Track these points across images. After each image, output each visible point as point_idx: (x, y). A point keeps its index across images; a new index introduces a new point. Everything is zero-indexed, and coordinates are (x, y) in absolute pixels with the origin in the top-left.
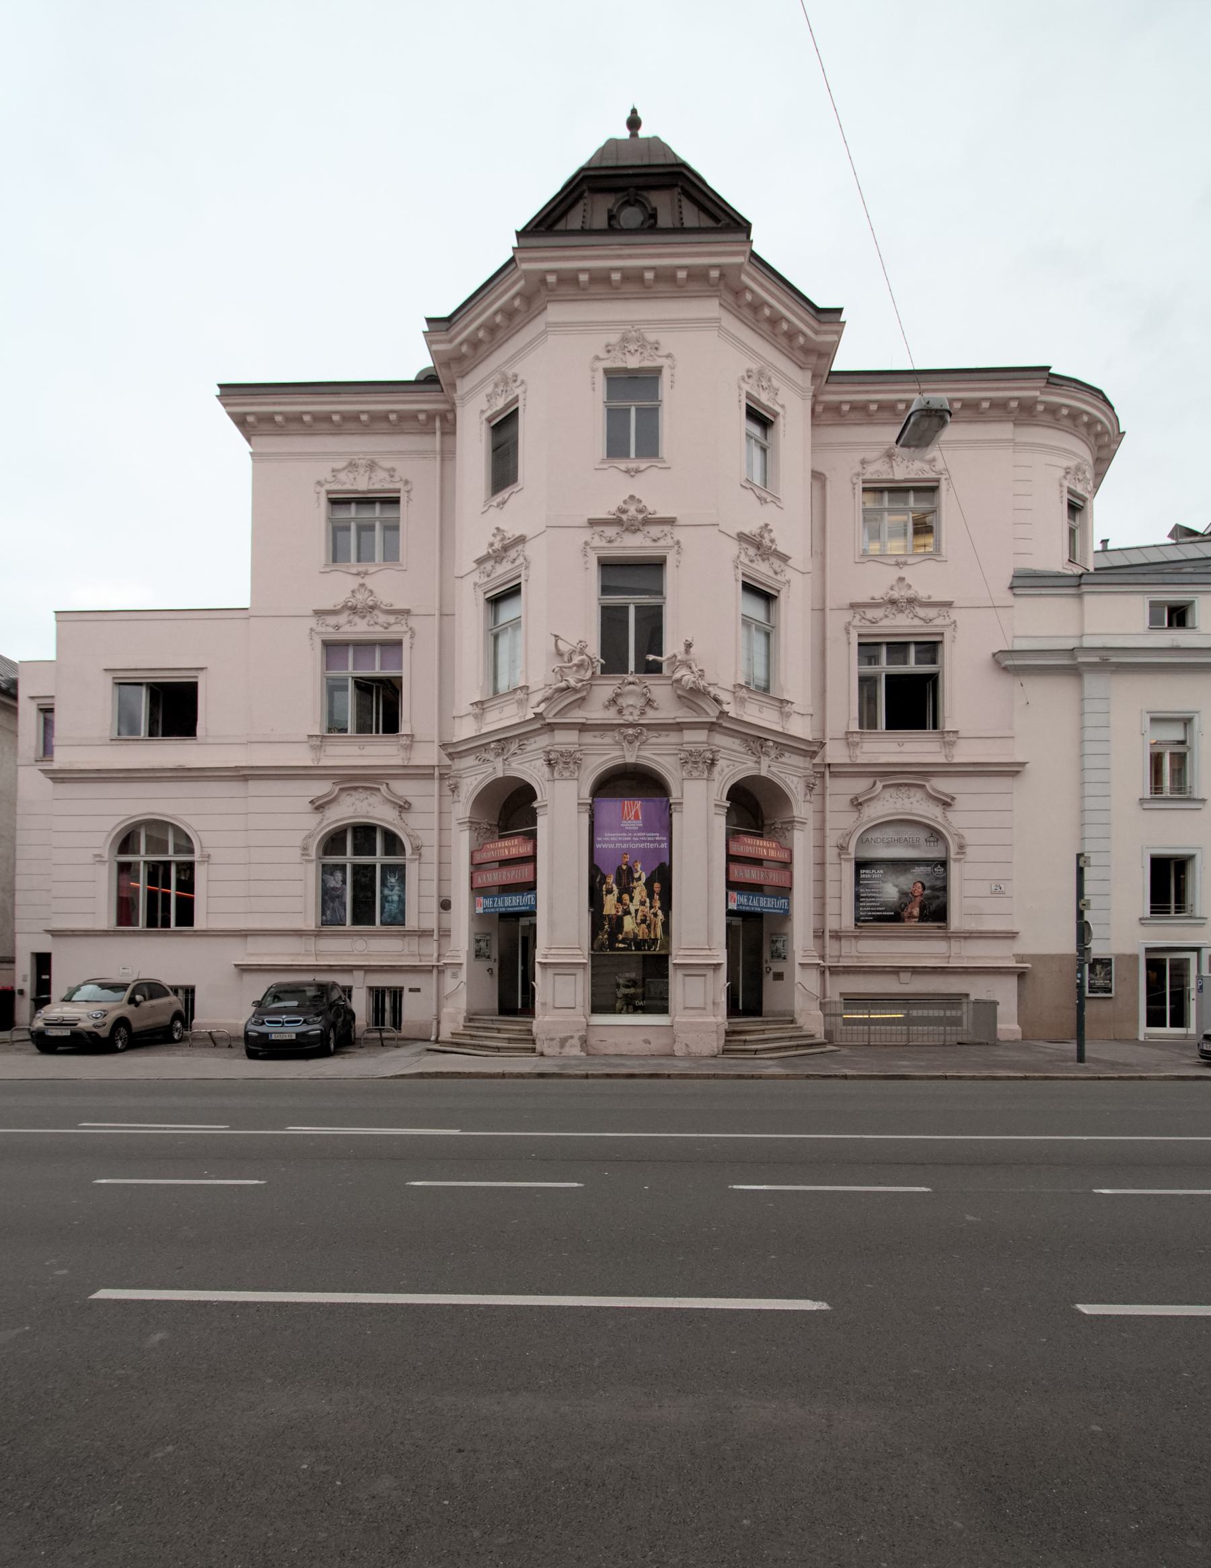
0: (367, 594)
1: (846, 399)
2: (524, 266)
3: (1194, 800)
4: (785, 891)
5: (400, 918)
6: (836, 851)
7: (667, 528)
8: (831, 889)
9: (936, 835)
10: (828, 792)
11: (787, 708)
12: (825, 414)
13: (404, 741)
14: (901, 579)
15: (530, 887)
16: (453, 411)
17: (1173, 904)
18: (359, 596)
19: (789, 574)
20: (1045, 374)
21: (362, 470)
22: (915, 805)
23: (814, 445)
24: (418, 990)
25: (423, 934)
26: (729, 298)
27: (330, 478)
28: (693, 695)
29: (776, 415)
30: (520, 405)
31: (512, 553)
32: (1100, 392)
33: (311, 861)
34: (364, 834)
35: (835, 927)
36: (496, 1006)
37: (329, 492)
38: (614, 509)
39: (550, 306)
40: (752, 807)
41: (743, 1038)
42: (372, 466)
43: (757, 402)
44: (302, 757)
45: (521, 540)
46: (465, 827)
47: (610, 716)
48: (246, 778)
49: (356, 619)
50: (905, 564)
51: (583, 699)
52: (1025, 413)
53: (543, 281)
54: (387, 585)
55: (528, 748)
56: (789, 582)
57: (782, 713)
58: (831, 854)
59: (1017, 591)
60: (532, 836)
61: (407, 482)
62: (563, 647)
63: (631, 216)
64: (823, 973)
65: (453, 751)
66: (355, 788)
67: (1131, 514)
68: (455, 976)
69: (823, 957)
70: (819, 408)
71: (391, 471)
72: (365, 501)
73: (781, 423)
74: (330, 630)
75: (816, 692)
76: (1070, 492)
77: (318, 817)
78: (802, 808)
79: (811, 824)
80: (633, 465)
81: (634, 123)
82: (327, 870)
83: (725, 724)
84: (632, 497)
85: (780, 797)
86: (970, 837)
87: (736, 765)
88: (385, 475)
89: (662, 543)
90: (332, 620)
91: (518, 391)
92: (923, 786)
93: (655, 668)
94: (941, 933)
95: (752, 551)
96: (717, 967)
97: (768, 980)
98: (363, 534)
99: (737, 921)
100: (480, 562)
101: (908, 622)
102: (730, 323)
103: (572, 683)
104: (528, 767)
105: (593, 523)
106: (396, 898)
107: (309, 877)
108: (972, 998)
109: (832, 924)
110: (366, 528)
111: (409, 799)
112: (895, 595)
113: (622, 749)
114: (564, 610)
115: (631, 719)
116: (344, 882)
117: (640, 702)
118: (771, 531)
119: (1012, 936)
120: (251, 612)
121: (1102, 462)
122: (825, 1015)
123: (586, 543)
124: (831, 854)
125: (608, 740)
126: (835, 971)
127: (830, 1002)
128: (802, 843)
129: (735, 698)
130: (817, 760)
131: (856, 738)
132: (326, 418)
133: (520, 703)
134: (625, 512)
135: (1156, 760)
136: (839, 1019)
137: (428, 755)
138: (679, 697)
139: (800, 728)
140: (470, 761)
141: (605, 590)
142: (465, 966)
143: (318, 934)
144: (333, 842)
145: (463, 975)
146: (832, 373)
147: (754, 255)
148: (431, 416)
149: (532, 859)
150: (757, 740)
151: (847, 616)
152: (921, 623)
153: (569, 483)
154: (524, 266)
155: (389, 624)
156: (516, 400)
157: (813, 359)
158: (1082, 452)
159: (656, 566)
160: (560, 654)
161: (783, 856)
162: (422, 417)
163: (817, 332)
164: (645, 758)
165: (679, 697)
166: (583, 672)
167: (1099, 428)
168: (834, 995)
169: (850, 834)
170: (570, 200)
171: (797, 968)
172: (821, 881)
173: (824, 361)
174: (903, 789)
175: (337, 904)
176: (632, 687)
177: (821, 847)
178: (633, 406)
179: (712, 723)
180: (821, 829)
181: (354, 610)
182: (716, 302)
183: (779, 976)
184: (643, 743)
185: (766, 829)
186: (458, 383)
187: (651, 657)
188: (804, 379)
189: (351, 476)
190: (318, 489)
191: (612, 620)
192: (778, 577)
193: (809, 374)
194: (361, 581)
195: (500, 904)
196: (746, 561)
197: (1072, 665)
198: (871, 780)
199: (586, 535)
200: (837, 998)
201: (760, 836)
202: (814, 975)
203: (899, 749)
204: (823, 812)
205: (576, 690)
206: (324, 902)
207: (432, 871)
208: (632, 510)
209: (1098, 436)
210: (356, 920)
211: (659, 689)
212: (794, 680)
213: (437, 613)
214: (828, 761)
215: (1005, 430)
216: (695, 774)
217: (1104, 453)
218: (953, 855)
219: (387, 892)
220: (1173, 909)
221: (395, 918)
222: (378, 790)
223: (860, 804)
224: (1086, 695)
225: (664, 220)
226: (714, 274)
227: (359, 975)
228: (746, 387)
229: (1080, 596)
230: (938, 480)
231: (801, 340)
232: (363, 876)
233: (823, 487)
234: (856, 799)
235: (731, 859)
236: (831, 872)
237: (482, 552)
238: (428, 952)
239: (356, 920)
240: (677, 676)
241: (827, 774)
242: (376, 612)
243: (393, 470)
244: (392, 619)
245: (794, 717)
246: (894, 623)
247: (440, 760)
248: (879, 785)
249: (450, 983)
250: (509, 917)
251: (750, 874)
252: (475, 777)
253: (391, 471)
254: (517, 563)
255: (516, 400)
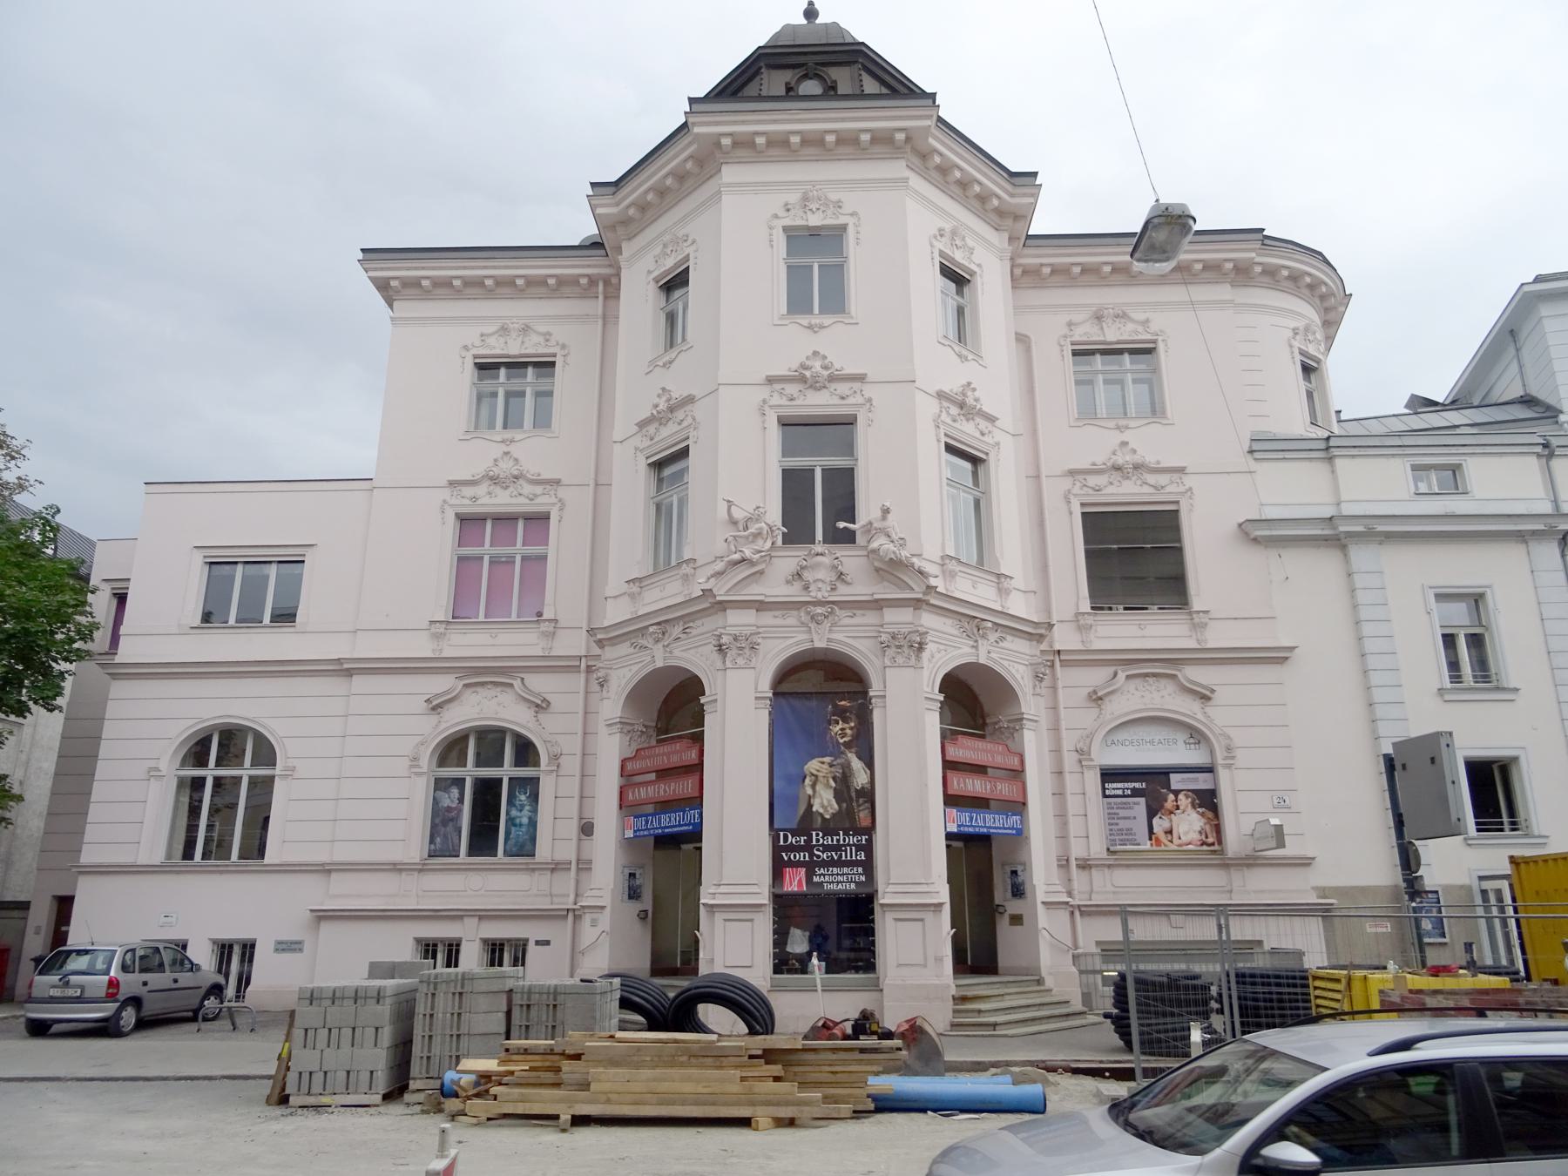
0: (511, 463)
1: (1050, 263)
2: (696, 130)
3: (1504, 689)
4: (1018, 806)
5: (528, 847)
6: (1076, 756)
7: (856, 386)
8: (1073, 805)
9: (1196, 735)
10: (1060, 684)
11: (1006, 584)
12: (1023, 277)
13: (544, 627)
14: (1124, 444)
15: (697, 801)
16: (618, 275)
17: (1505, 819)
18: (501, 464)
19: (998, 436)
20: (1259, 236)
21: (514, 334)
22: (1164, 698)
23: (1015, 307)
24: (547, 943)
25: (556, 867)
26: (916, 161)
27: (478, 343)
28: (892, 568)
29: (973, 273)
30: (691, 263)
31: (680, 415)
32: (1320, 254)
33: (421, 774)
34: (490, 741)
35: (1082, 854)
36: (647, 965)
37: (475, 357)
38: (795, 366)
39: (724, 168)
40: (970, 702)
41: (992, 1019)
42: (526, 330)
43: (952, 260)
44: (421, 647)
45: (690, 400)
46: (615, 729)
47: (793, 592)
48: (349, 673)
49: (498, 490)
50: (1127, 428)
51: (761, 572)
52: (1242, 274)
53: (718, 145)
54: (535, 453)
55: (694, 632)
56: (998, 444)
57: (999, 590)
58: (1070, 760)
59: (1257, 455)
60: (698, 739)
61: (564, 347)
62: (738, 514)
63: (811, 87)
64: (1072, 913)
65: (603, 638)
66: (483, 684)
67: (1401, 353)
68: (594, 923)
69: (1070, 894)
70: (1018, 271)
71: (547, 336)
72: (516, 366)
73: (978, 281)
74: (467, 502)
75: (1034, 567)
76: (1302, 353)
77: (434, 719)
78: (1031, 704)
79: (1044, 723)
80: (815, 321)
81: (811, 13)
82: (441, 785)
83: (933, 601)
84: (815, 353)
85: (1004, 690)
86: (1238, 737)
87: (948, 650)
88: (541, 339)
89: (851, 401)
90: (468, 491)
91: (690, 250)
92: (1174, 677)
93: (849, 538)
94: (1215, 859)
95: (954, 410)
96: (938, 906)
97: (1004, 929)
98: (512, 400)
99: (958, 844)
100: (642, 425)
101: (1137, 489)
102: (916, 182)
103: (748, 553)
104: (694, 657)
105: (771, 380)
106: (525, 821)
107: (419, 793)
108: (1267, 947)
109: (1077, 851)
110: (514, 395)
111: (548, 697)
112: (1120, 460)
113: (810, 631)
114: (742, 474)
115: (820, 596)
116: (461, 800)
117: (830, 576)
118: (974, 390)
119: (1305, 863)
120: (374, 484)
121: (1331, 324)
122: (1081, 972)
123: (764, 401)
124: (1070, 760)
125: (791, 621)
126: (1088, 911)
127: (1086, 955)
128: (1033, 744)
129: (943, 572)
130: (1044, 646)
131: (1090, 620)
132: (478, 283)
133: (686, 578)
134: (807, 368)
135: (1449, 640)
136: (1099, 977)
137: (573, 644)
138: (877, 570)
139: (1019, 606)
140: (624, 649)
141: (787, 451)
142: (608, 911)
143: (422, 869)
144: (452, 749)
145: (605, 920)
146: (1029, 237)
147: (940, 119)
148: (593, 281)
149: (697, 768)
150: (973, 621)
151: (1067, 483)
152: (1152, 490)
153: (748, 335)
154: (696, 130)
155: (536, 496)
156: (687, 258)
157: (1009, 222)
158: (1309, 314)
159: (849, 422)
160: (734, 523)
161: (1014, 762)
162: (584, 281)
163: (1012, 195)
164: (839, 642)
165: (877, 570)
166: (760, 542)
167: (1324, 289)
168: (1087, 945)
169: (1091, 736)
170: (747, 75)
171: (1040, 909)
172: (1060, 794)
173: (1020, 225)
174: (1151, 680)
175: (450, 828)
176: (819, 558)
177: (1057, 751)
178: (816, 263)
179: (918, 600)
180: (1055, 729)
181: (494, 480)
182: (903, 163)
183: (1017, 920)
184: (834, 624)
185: (989, 729)
186: (624, 245)
187: (842, 525)
188: (999, 240)
189: (502, 340)
190: (464, 353)
191: (795, 484)
192: (985, 438)
193: (1006, 235)
194: (506, 449)
195: (656, 825)
196: (949, 421)
197: (1334, 536)
198: (1111, 670)
199: (764, 392)
200: (1094, 950)
201: (983, 737)
202: (1064, 915)
203: (1140, 633)
204: (1054, 708)
205: (751, 563)
206: (434, 826)
207: (571, 786)
208: (817, 365)
209: (1323, 298)
210: (473, 850)
211: (849, 559)
212: (1012, 552)
213: (592, 483)
214: (1057, 647)
215: (1224, 292)
216: (900, 660)
217: (1331, 316)
218: (1220, 761)
219: (514, 813)
220: (1506, 826)
221: (522, 846)
222: (511, 685)
223: (1100, 699)
224: (1355, 568)
225: (842, 89)
226: (900, 136)
227: (471, 923)
228: (939, 245)
229: (1330, 459)
230: (1155, 342)
231: (996, 202)
232: (487, 793)
233: (1028, 350)
234: (1095, 692)
235: (949, 765)
236: (1071, 782)
237: (645, 414)
238: (561, 892)
239: (473, 850)
240: (874, 545)
241: (1057, 664)
242: (521, 481)
243: (550, 334)
244: (538, 489)
245: (1015, 595)
246: (1121, 490)
247: (588, 649)
248: (1122, 676)
249: (588, 933)
250: (668, 842)
251: (973, 786)
252: (627, 670)
253: (547, 336)
254: (685, 424)
255: (687, 258)
